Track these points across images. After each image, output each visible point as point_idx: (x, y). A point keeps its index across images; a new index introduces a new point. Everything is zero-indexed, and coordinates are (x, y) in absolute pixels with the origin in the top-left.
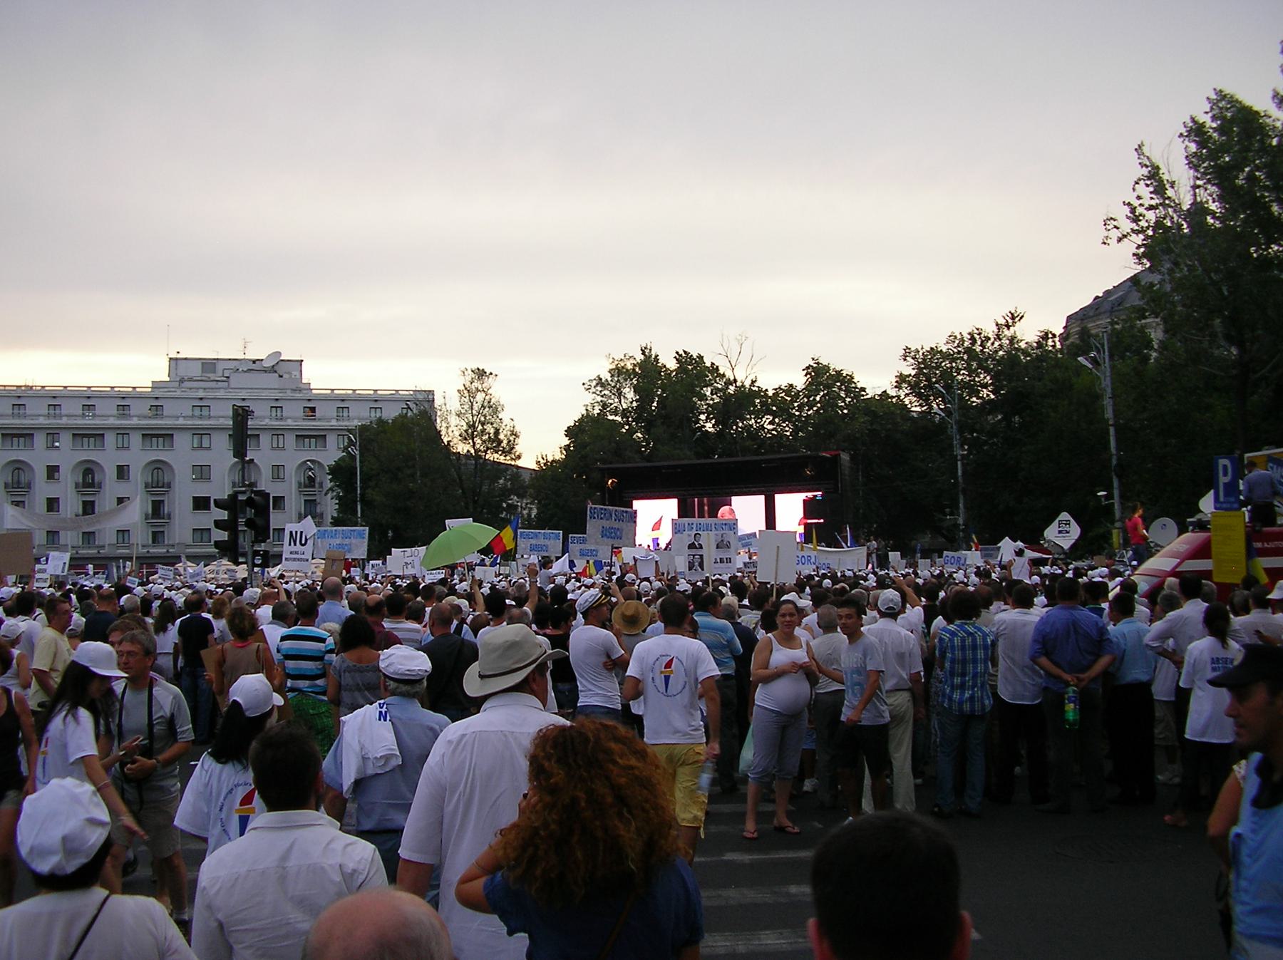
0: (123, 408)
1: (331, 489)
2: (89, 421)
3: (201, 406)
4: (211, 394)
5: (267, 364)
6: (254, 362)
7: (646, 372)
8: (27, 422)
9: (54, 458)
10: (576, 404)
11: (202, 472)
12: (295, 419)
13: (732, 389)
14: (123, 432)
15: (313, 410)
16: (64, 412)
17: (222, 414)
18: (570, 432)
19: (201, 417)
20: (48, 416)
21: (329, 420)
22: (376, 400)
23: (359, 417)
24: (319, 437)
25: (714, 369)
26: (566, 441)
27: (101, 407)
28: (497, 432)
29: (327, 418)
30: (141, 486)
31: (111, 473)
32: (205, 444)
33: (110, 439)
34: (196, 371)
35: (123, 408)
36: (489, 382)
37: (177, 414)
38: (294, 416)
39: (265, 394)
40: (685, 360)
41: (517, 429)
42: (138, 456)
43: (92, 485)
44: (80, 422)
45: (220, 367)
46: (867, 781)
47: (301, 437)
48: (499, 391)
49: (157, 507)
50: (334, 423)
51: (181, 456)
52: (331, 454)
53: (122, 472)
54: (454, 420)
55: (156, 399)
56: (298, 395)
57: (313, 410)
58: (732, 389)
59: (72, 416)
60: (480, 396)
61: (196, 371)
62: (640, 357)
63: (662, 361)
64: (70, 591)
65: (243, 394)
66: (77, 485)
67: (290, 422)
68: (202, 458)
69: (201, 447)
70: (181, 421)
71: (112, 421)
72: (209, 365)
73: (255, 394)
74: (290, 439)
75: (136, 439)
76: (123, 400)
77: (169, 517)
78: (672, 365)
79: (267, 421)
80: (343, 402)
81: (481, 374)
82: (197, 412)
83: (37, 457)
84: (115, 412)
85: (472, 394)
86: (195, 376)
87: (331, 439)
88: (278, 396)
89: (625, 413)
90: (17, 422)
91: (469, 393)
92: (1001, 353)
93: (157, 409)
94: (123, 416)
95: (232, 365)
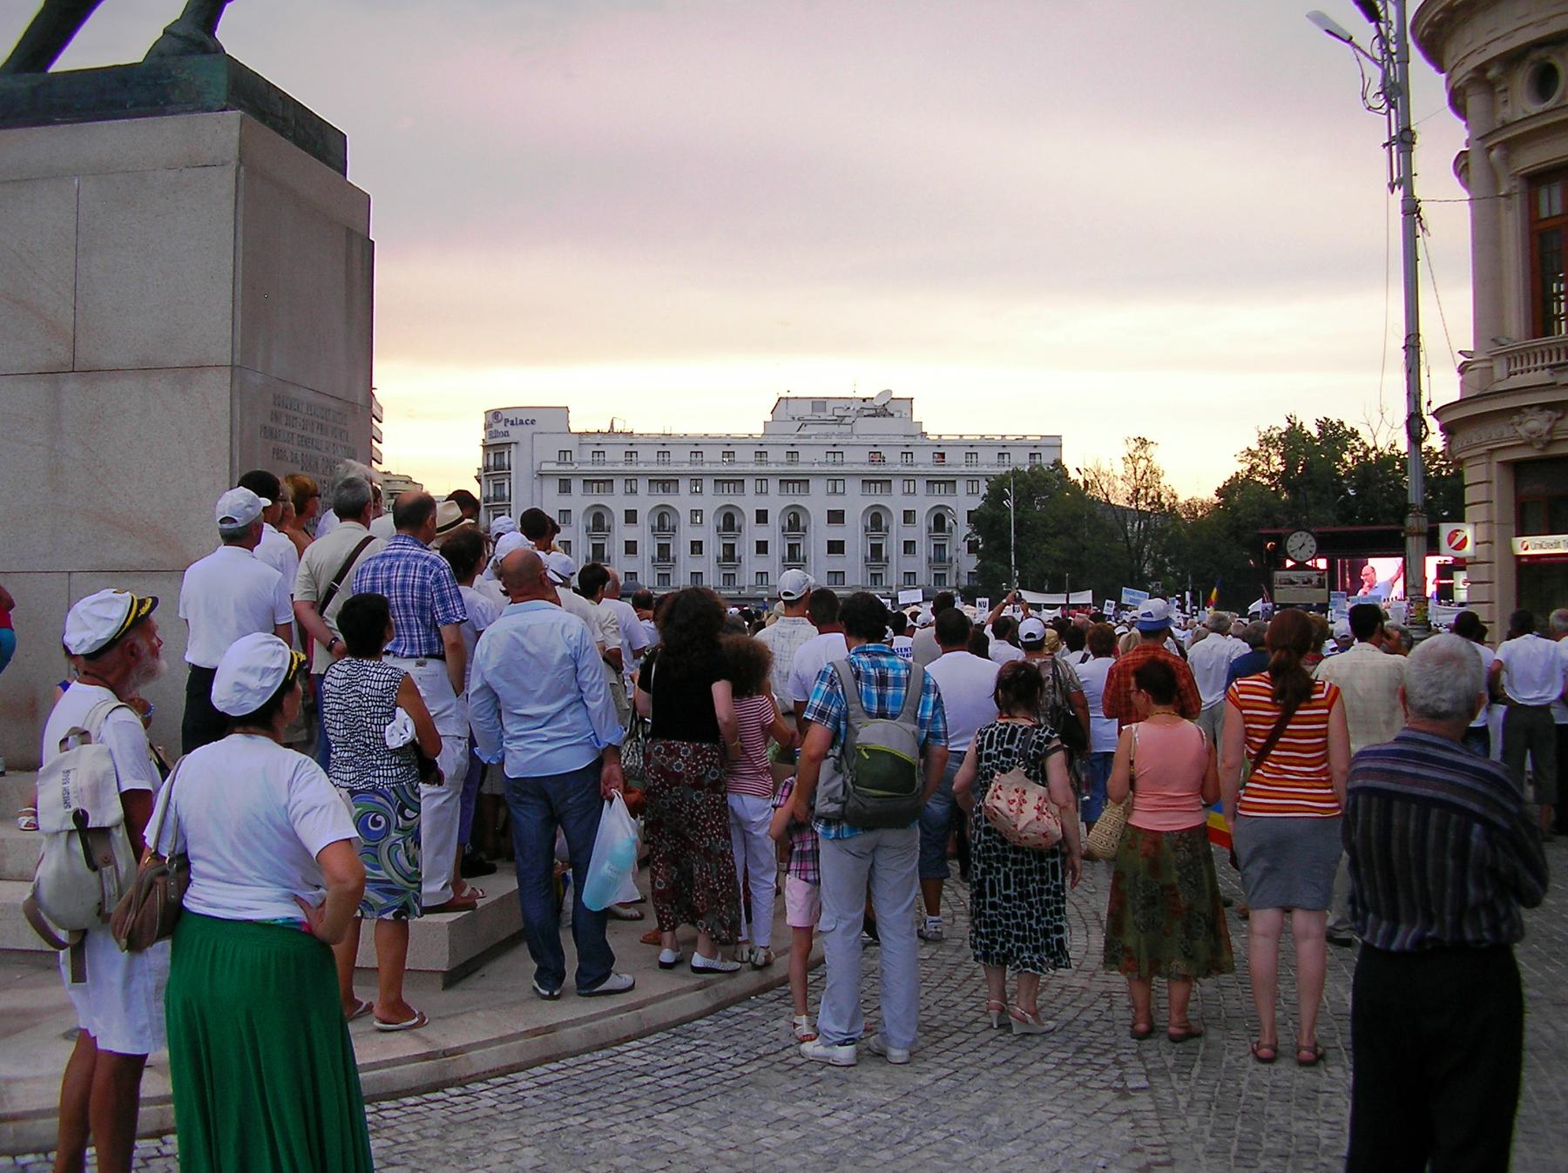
3: (835, 452)
5: (879, 403)
7: (1293, 439)
8: (672, 468)
9: (697, 503)
10: (1228, 467)
13: (1372, 456)
14: (762, 478)
15: (943, 455)
20: (691, 463)
22: (1003, 448)
23: (988, 464)
24: (949, 483)
25: (1354, 434)
28: (1159, 496)
29: (956, 462)
31: (751, 517)
32: (840, 489)
33: (750, 484)
34: (806, 411)
36: (1151, 448)
38: (924, 461)
40: (1324, 425)
42: (646, 501)
44: (723, 468)
47: (868, 482)
48: (1160, 457)
50: (963, 468)
54: (1119, 484)
57: (943, 455)
58: (1372, 456)
59: (712, 462)
60: (1142, 464)
62: (1285, 426)
63: (1306, 428)
64: (1154, 578)
65: (875, 441)
67: (920, 468)
70: (816, 467)
73: (886, 440)
74: (921, 485)
75: (774, 485)
80: (972, 448)
81: (1143, 443)
83: (682, 501)
84: (784, 459)
86: (804, 416)
88: (909, 441)
89: (1271, 476)
94: (761, 462)
95: (842, 403)
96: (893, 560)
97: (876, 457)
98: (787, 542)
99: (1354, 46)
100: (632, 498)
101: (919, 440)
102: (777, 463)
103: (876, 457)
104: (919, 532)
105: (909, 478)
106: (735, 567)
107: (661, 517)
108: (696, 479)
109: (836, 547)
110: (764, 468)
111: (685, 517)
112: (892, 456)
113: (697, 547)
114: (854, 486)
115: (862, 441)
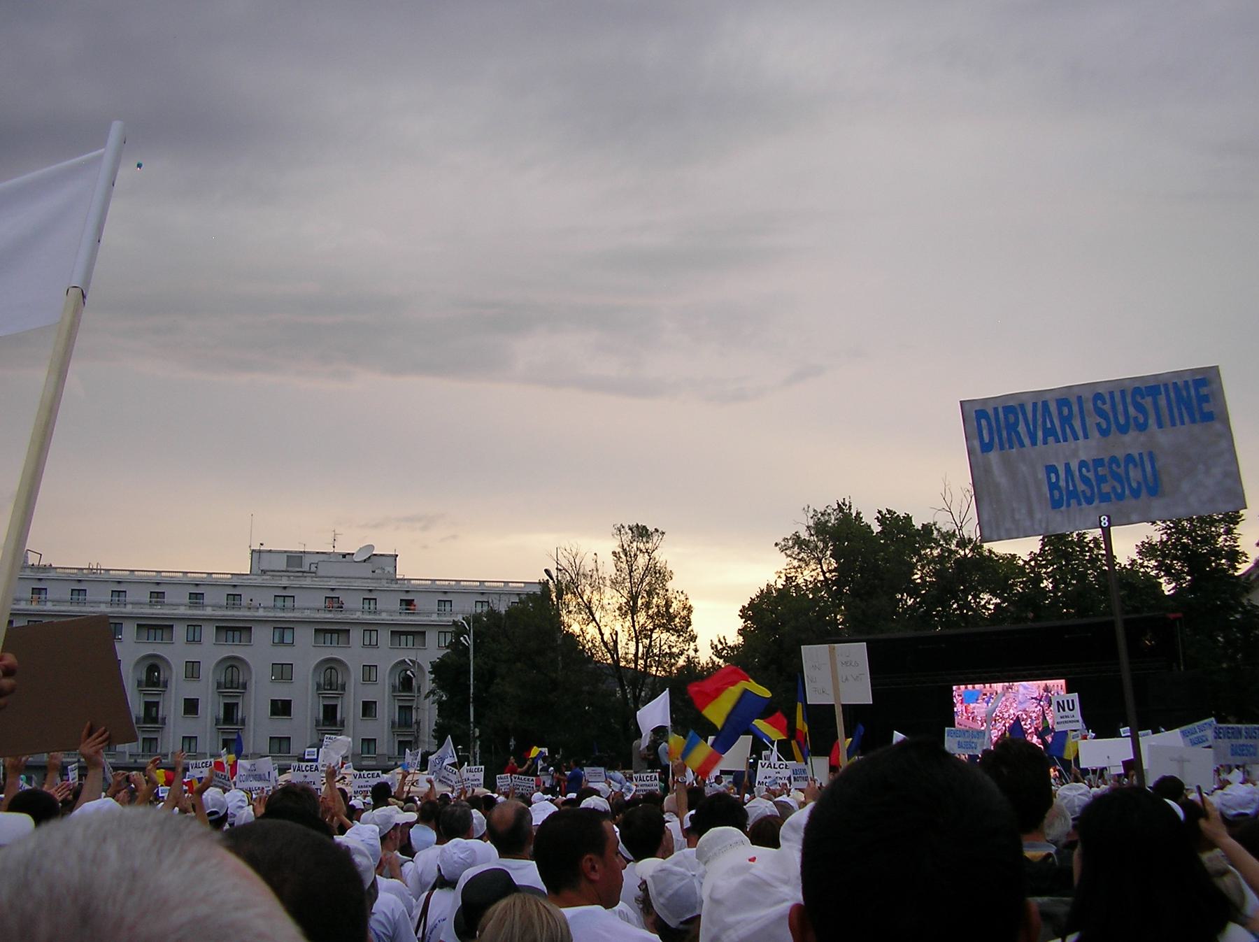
0: (196, 598)
1: (432, 692)
2: (158, 610)
3: (284, 596)
4: (296, 583)
6: (344, 556)
9: (194, 653)
11: (283, 672)
12: (390, 612)
15: (161, 595)
16: (128, 599)
17: (307, 605)
18: (744, 613)
19: (283, 609)
20: (111, 603)
21: (430, 614)
22: (482, 592)
23: (463, 609)
24: (418, 634)
26: (740, 623)
27: (171, 596)
28: (668, 605)
29: (427, 611)
30: (211, 686)
32: (288, 639)
35: (196, 598)
37: (262, 605)
38: (389, 609)
39: (357, 584)
41: (690, 602)
42: (211, 651)
43: (156, 684)
44: (147, 611)
45: (307, 561)
46: (517, 918)
47: (398, 633)
48: (666, 554)
49: (230, 710)
50: (434, 617)
51: (259, 653)
52: (433, 651)
53: (193, 670)
55: (234, 589)
56: (394, 586)
57: (161, 595)
59: (138, 603)
61: (281, 564)
65: (333, 583)
66: (139, 684)
67: (384, 616)
68: (283, 655)
69: (282, 642)
70: (261, 613)
71: (182, 611)
72: (295, 558)
73: (345, 584)
74: (385, 636)
76: (197, 590)
77: (243, 721)
78: (876, 528)
79: (358, 614)
80: (445, 594)
81: (641, 532)
82: (280, 603)
83: (353, 654)
84: (187, 600)
85: (631, 558)
87: (432, 637)
88: (372, 585)
90: (75, 609)
91: (625, 555)
92: (990, 601)
93: (234, 598)
96: (171, 721)
97: (334, 602)
98: (222, 701)
99: (77, 314)
100: (195, 648)
101: (384, 584)
102: (214, 606)
103: (334, 602)
104: (382, 693)
105: (370, 628)
106: (157, 730)
107: (153, 668)
108: (194, 625)
109: (281, 708)
110: (197, 612)
111: (356, 674)
112: (353, 602)
113: (191, 706)
114: (305, 636)
115: (317, 583)
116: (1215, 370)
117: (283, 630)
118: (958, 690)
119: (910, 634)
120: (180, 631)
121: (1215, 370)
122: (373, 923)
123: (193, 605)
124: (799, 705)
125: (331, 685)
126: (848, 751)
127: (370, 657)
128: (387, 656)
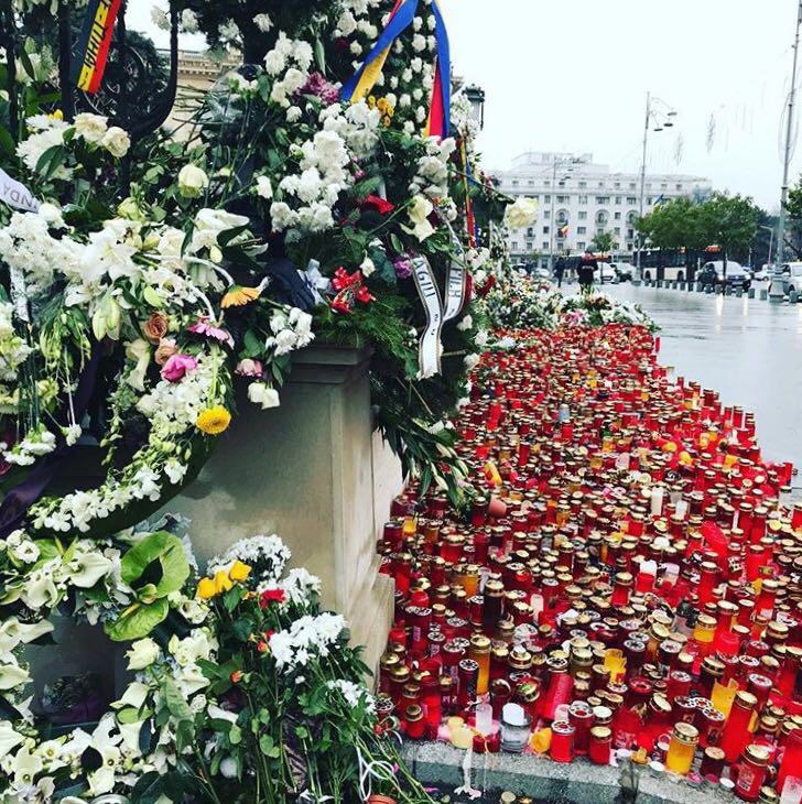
51: (572, 207)
61: (539, 159)
68: (584, 208)
71: (543, 190)
83: (610, 207)
107: (600, 215)
112: (625, 186)
114: (592, 200)
116: (89, 747)
117: (583, 199)
118: (666, 269)
119: (464, 163)
120: (613, 200)
121: (89, 747)
122: (340, 400)
123: (514, 187)
124: (281, 382)
125: (562, 221)
126: (20, 666)
127: (617, 208)
128: (625, 208)
